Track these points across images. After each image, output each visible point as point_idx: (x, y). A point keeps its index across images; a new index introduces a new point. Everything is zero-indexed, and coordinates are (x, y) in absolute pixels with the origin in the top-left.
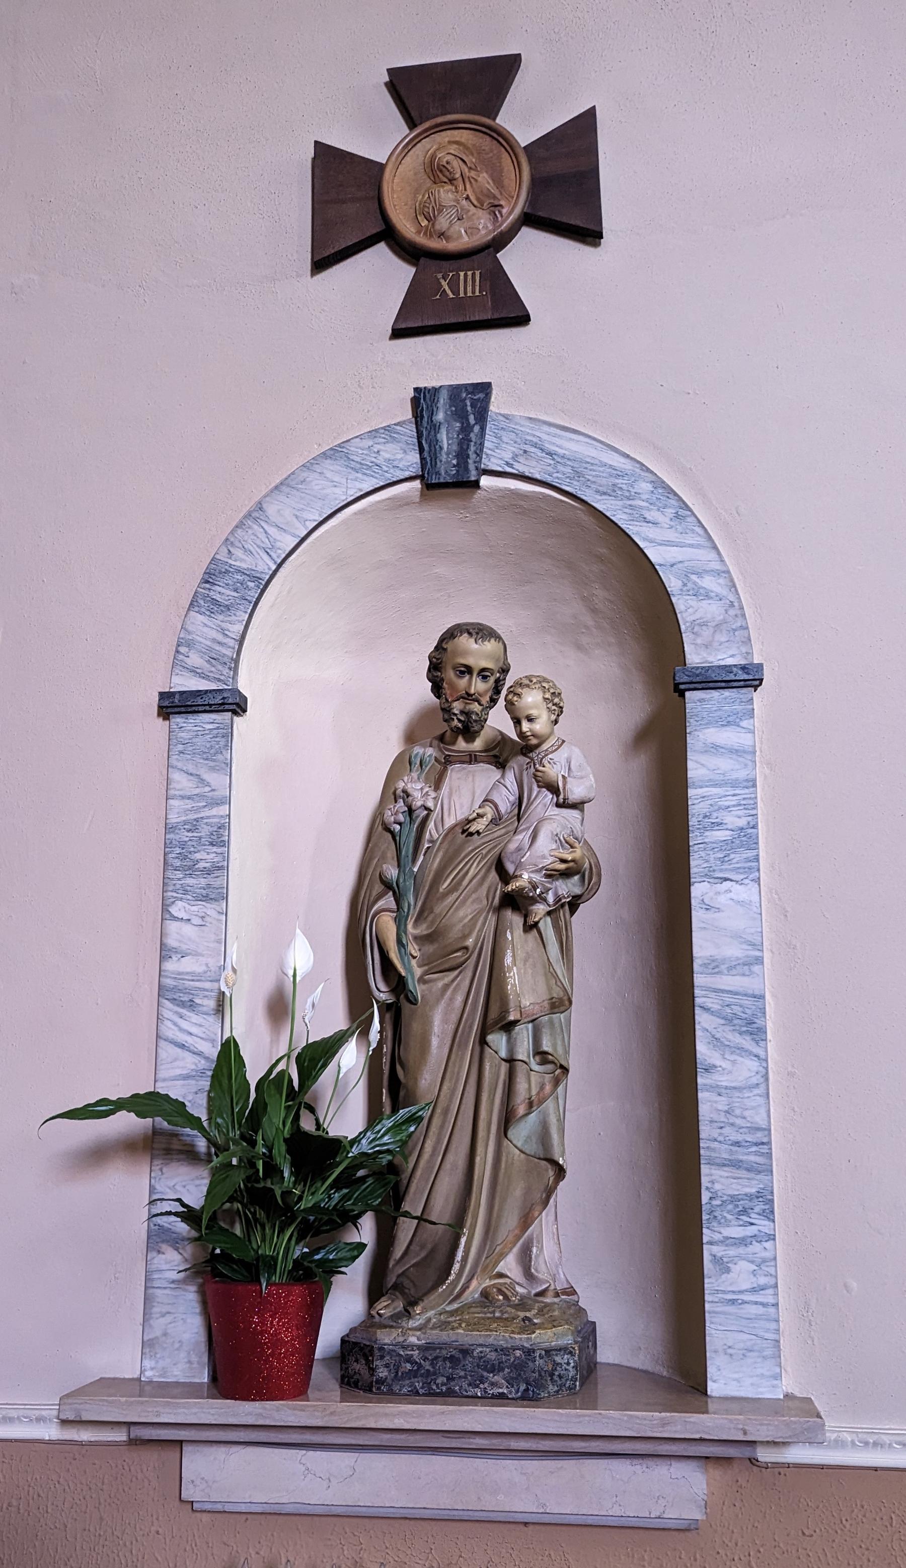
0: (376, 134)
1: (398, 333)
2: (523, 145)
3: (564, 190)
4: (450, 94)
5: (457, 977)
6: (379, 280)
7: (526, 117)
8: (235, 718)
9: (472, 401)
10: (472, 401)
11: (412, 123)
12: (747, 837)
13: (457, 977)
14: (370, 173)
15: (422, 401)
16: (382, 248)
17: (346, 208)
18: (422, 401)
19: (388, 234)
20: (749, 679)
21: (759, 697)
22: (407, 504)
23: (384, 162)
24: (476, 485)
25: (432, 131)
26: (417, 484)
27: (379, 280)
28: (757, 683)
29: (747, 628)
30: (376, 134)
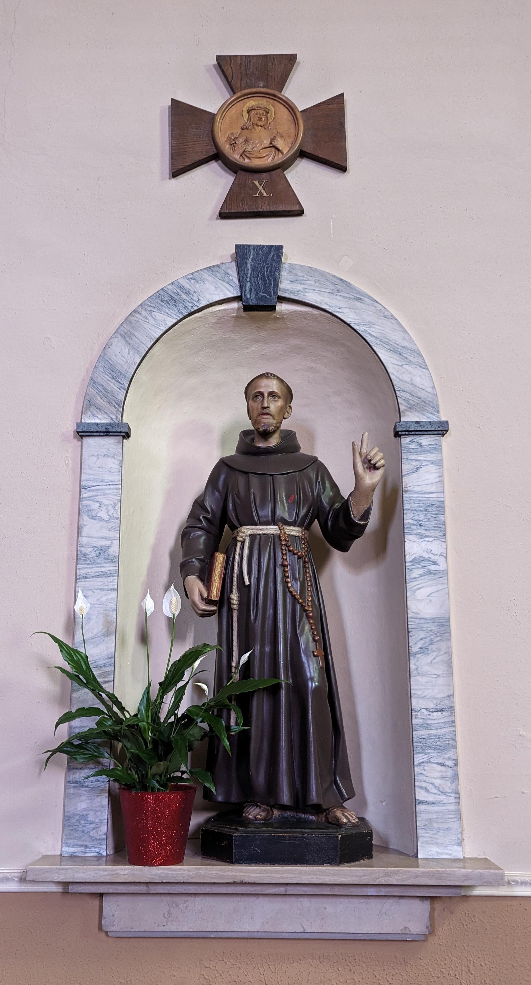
0: (210, 97)
1: (223, 216)
2: (300, 110)
3: (324, 137)
4: (256, 76)
5: (337, 312)
6: (211, 184)
7: (303, 92)
8: (125, 441)
9: (272, 256)
10: (272, 256)
11: (233, 90)
12: (443, 623)
13: (337, 312)
14: (209, 118)
15: (242, 252)
16: (214, 165)
17: (191, 140)
18: (242, 252)
19: (218, 156)
20: (441, 430)
21: (446, 441)
22: (103, 538)
23: (216, 113)
24: (273, 308)
25: (233, 104)
26: (235, 305)
27: (211, 184)
28: (445, 432)
29: (451, 709)
30: (210, 97)
